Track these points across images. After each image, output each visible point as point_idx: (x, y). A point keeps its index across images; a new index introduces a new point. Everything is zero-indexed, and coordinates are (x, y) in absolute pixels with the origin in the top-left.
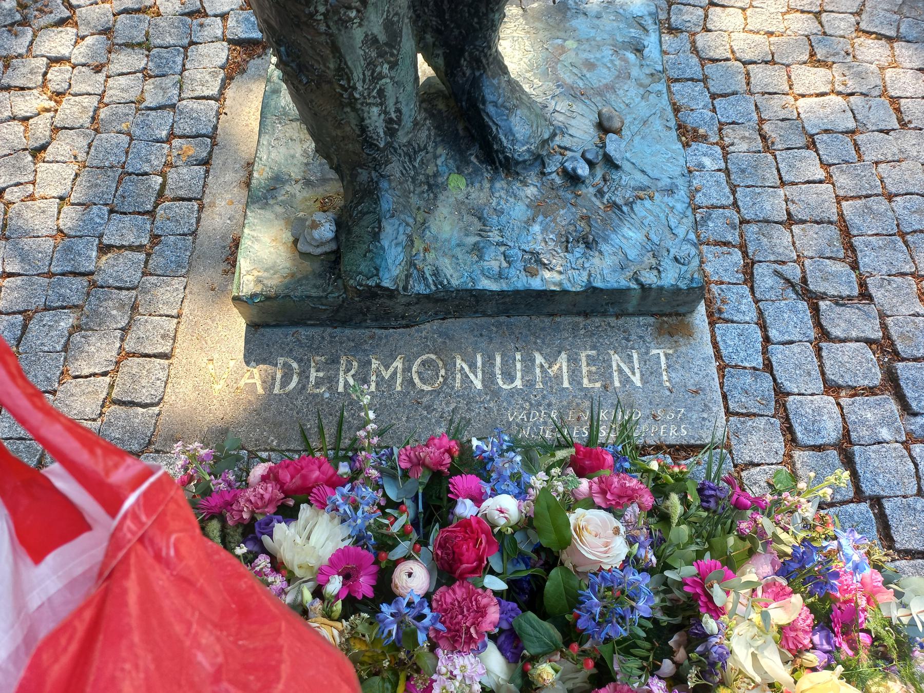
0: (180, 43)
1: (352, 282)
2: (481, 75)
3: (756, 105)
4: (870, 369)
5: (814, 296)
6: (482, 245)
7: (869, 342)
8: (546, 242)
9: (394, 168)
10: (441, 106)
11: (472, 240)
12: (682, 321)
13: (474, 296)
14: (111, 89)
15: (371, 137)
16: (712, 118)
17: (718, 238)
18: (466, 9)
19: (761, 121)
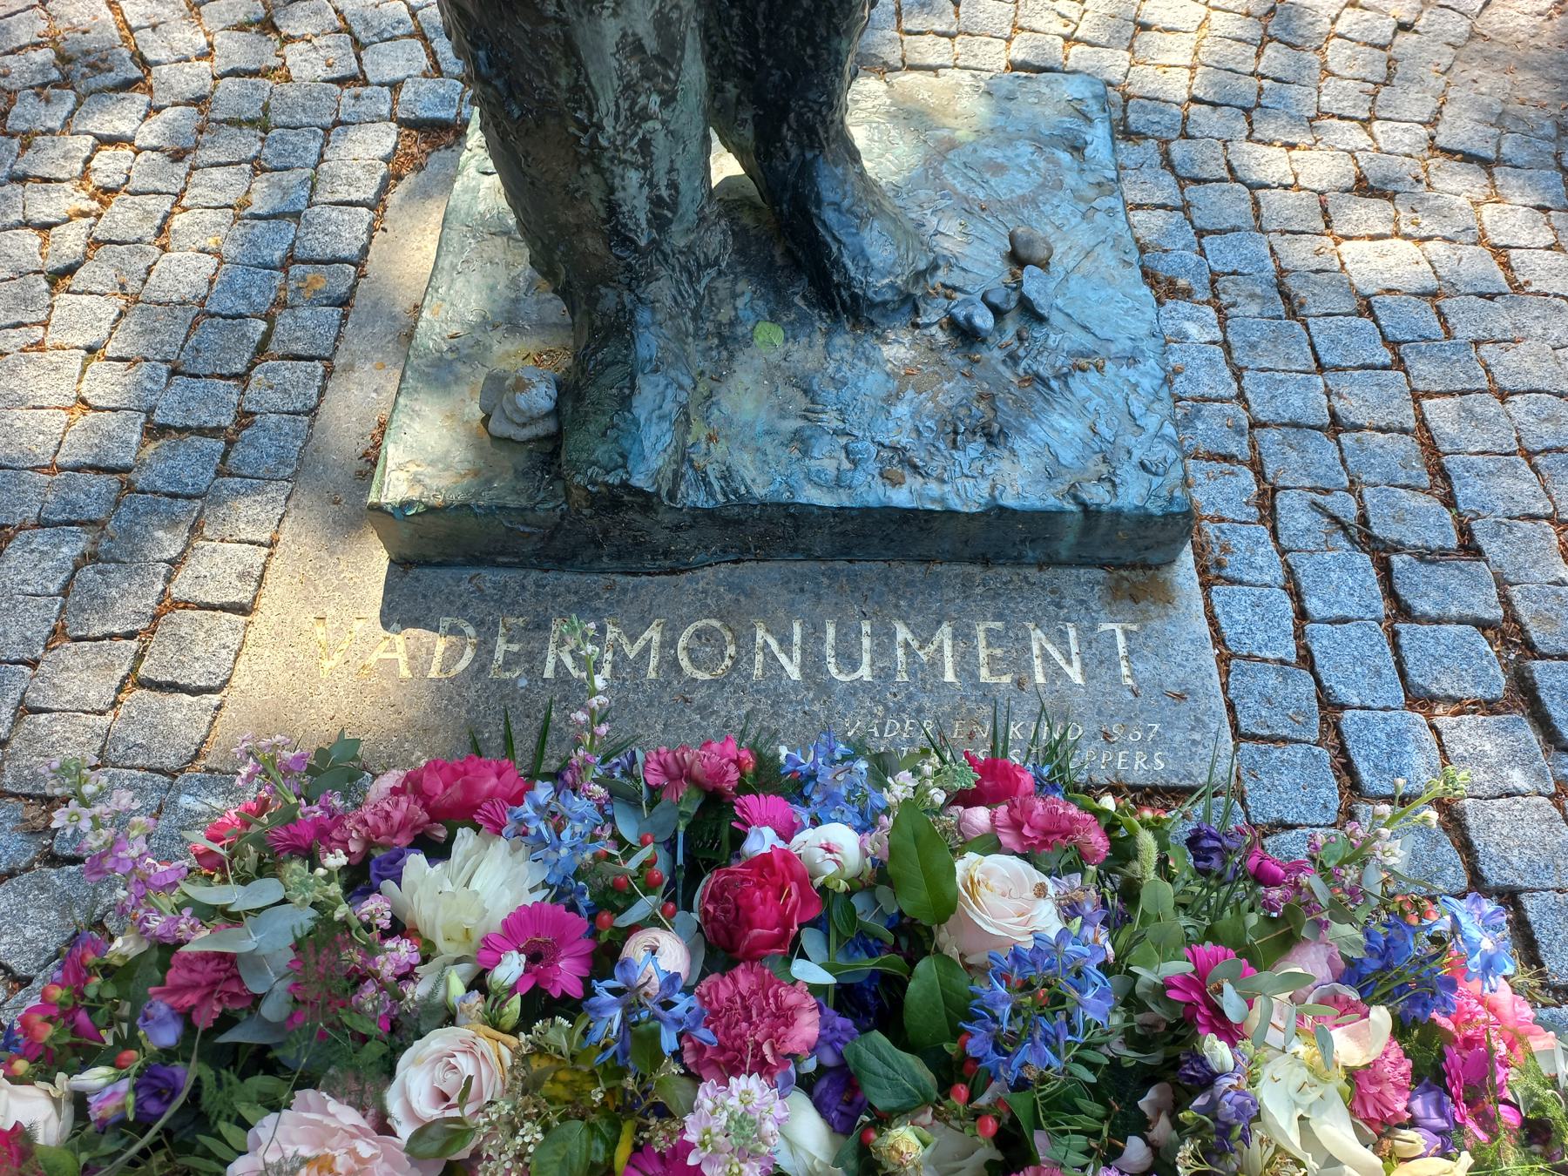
0: (319, 121)
1: (578, 478)
2: (816, 157)
3: (1272, 249)
4: (1485, 670)
5: (1381, 547)
6: (808, 433)
7: (1482, 625)
8: (919, 433)
9: (662, 289)
10: (747, 219)
11: (793, 424)
12: (1153, 578)
13: (792, 515)
14: (196, 185)
15: (626, 225)
16: (1199, 264)
17: (1213, 448)
18: (793, 30)
19: (1282, 272)
